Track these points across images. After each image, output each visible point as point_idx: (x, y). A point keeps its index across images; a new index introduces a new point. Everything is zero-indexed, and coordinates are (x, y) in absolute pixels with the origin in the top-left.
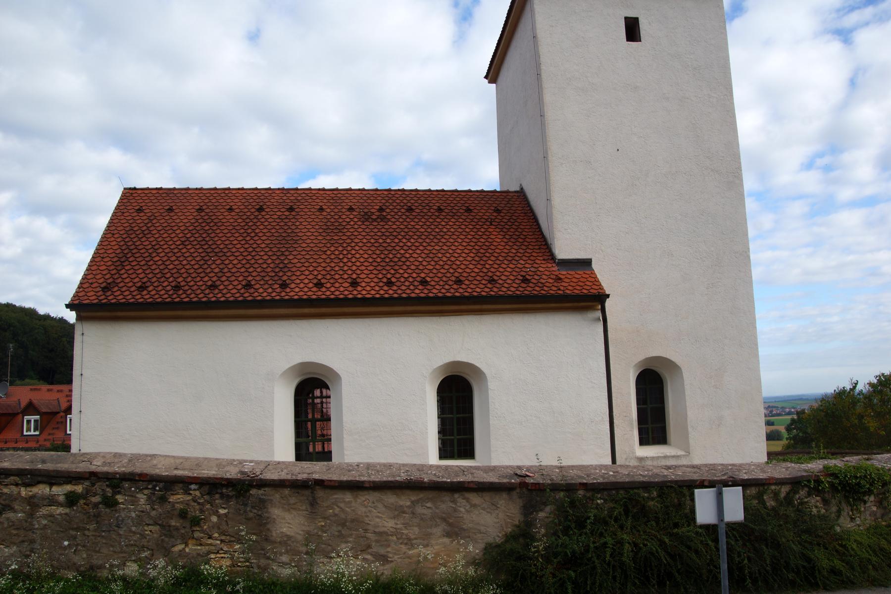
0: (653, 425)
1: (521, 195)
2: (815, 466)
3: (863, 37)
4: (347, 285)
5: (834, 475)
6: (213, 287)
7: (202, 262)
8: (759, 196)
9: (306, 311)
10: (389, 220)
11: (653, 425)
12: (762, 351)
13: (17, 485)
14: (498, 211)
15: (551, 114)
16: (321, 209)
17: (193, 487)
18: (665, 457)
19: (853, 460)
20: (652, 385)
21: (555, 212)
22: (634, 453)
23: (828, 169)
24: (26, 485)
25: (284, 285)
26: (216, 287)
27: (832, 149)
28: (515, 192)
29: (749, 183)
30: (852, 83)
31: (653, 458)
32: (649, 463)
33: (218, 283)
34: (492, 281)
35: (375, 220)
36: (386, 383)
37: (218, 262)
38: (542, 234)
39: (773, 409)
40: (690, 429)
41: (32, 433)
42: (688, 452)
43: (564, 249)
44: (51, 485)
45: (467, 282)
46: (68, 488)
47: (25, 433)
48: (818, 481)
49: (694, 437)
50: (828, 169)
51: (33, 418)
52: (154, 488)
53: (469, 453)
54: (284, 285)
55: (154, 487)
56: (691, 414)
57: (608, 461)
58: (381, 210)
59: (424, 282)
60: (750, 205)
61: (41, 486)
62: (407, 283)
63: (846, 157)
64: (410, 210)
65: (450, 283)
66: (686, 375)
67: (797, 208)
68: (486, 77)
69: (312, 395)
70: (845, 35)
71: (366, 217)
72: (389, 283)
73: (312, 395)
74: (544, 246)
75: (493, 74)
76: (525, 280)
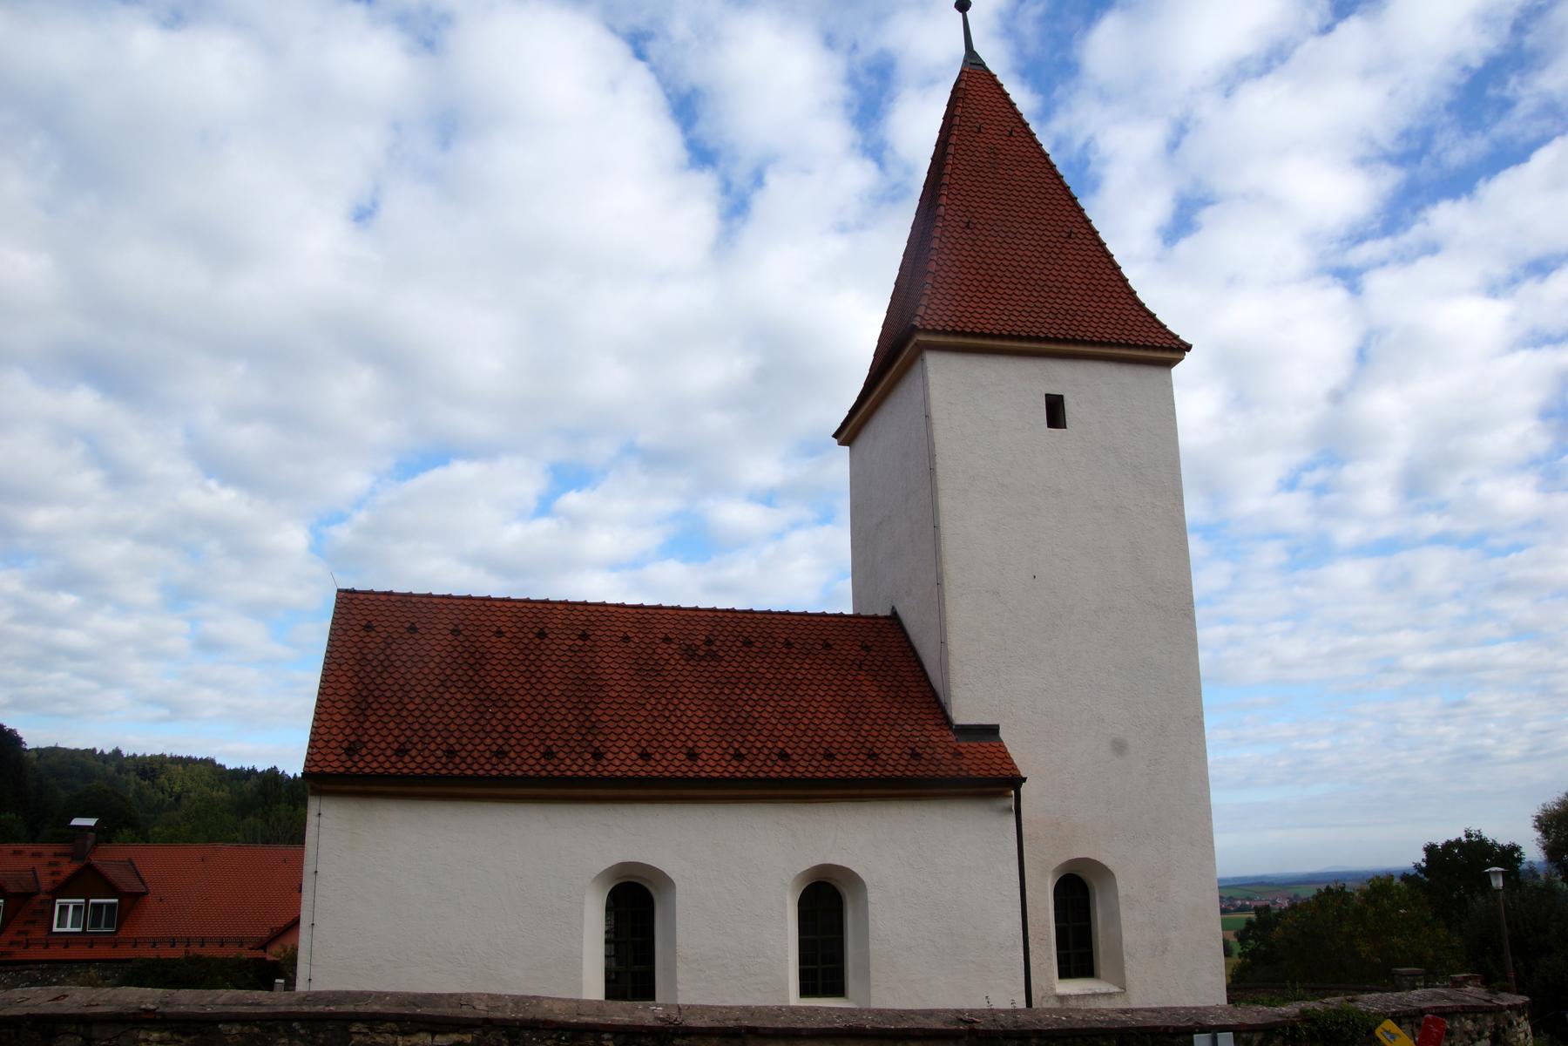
0: (1077, 954)
1: (894, 621)
2: (1290, 1009)
3: (1381, 284)
4: (682, 757)
5: (1312, 1021)
6: (501, 754)
7: (476, 716)
8: (1208, 532)
9: (632, 792)
10: (722, 658)
11: (1077, 954)
12: (1217, 798)
13: (393, 1033)
14: (867, 648)
15: (948, 527)
16: (626, 639)
17: (606, 1036)
18: (1094, 995)
19: (1334, 1002)
20: (1077, 895)
21: (951, 661)
22: (1053, 989)
23: (1320, 490)
24: (404, 1033)
25: (598, 755)
26: (505, 754)
27: (1332, 449)
28: (886, 617)
29: (1194, 509)
30: (1362, 356)
31: (1078, 997)
32: (1073, 1004)
33: (506, 748)
34: (872, 756)
35: (702, 658)
36: (730, 890)
37: (499, 716)
38: (930, 685)
39: (1233, 897)
40: (1126, 958)
41: (69, 929)
42: (1124, 988)
43: (964, 711)
44: (434, 1034)
45: (840, 757)
46: (455, 1037)
47: (55, 929)
48: (1294, 1028)
49: (1132, 969)
50: (1320, 490)
51: (71, 902)
52: (559, 1038)
53: (838, 990)
54: (598, 755)
55: (559, 1038)
56: (1128, 937)
57: (1021, 1003)
58: (709, 642)
59: (784, 756)
60: (1195, 546)
61: (422, 1035)
62: (762, 757)
63: (1350, 473)
64: (748, 643)
65: (819, 757)
66: (1120, 882)
67: (1271, 554)
68: (836, 436)
69: (634, 907)
70: (1350, 278)
71: (690, 653)
72: (739, 756)
73: (634, 907)
74: (936, 707)
75: (848, 433)
76: (915, 755)
